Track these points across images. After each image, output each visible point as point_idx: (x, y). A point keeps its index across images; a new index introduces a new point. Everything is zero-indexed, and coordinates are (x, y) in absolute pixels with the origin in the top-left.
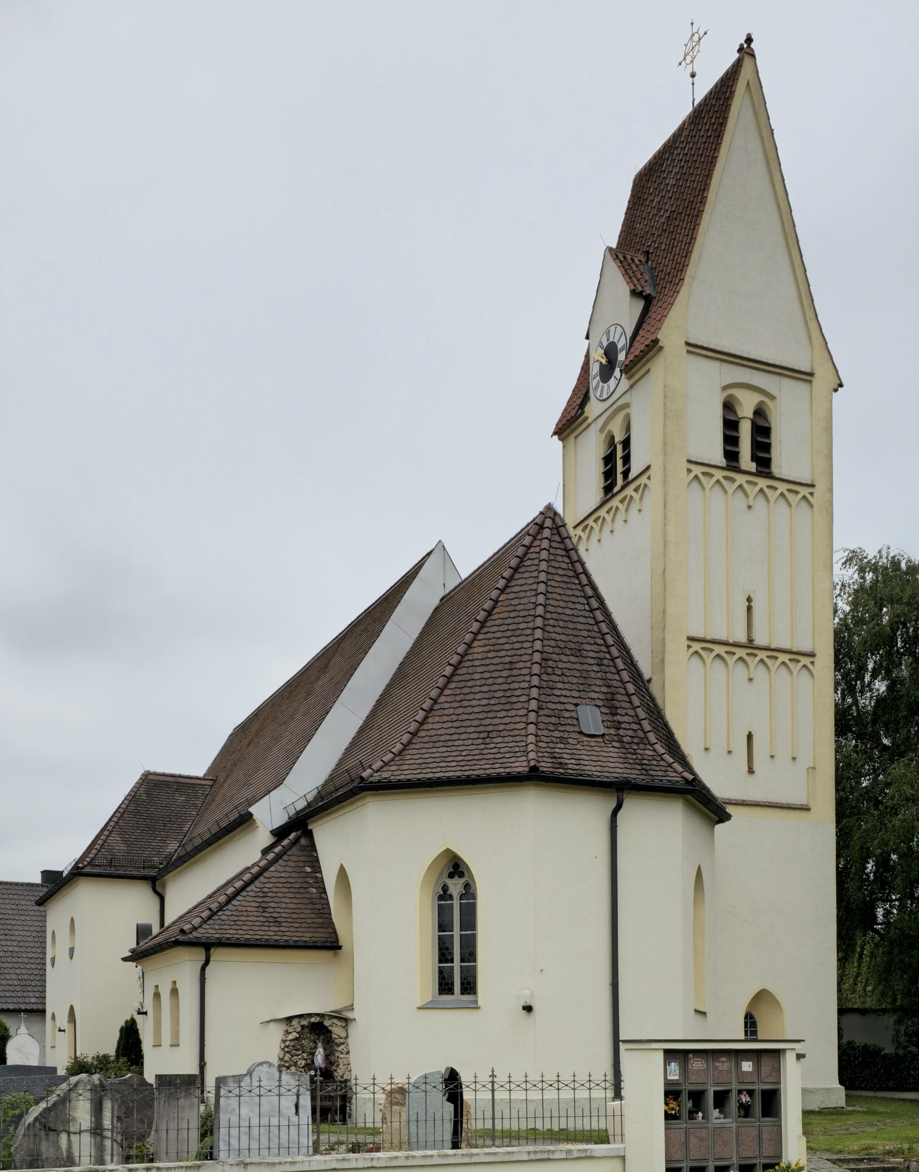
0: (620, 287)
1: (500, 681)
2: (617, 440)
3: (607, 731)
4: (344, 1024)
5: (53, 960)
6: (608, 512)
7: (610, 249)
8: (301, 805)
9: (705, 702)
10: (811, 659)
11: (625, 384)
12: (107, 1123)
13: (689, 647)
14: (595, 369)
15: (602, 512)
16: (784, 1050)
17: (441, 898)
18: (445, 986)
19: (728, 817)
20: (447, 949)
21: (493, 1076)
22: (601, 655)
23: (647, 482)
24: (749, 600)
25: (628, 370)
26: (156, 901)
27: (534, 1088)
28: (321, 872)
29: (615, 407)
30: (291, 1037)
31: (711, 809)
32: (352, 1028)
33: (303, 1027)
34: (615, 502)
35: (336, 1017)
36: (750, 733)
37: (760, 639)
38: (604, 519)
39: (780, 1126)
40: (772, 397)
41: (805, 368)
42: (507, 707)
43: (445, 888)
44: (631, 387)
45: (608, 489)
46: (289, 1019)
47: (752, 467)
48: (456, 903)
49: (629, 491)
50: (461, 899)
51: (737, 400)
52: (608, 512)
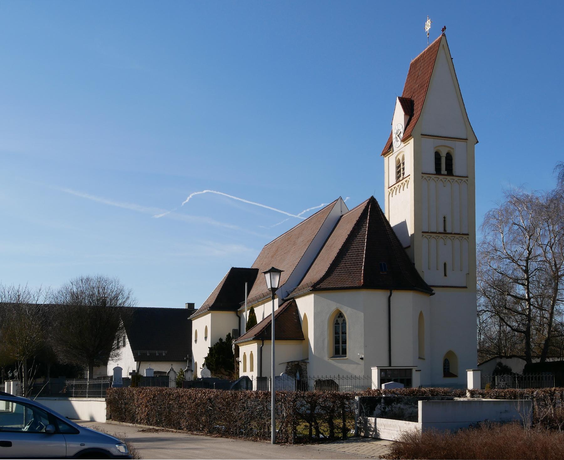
11: (403, 144)
17: (335, 324)
26: (238, 318)
32: (308, 365)
34: (400, 183)
40: (453, 149)
41: (464, 137)
43: (337, 321)
45: (398, 178)
46: (288, 363)
47: (446, 173)
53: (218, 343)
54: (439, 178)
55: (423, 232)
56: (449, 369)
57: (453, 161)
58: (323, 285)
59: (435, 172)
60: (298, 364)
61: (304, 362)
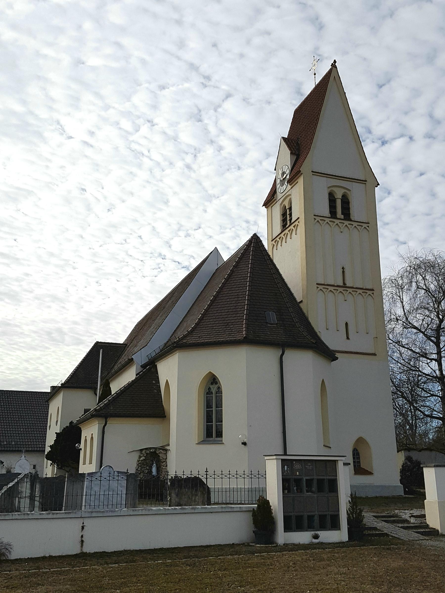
0: (287, 152)
1: (233, 302)
2: (287, 208)
3: (279, 322)
4: (165, 452)
5: (50, 426)
6: (284, 235)
7: (283, 138)
8: (153, 354)
9: (326, 309)
10: (372, 292)
11: (289, 187)
12: (37, 493)
13: (318, 287)
14: (278, 181)
15: (282, 235)
16: (338, 460)
17: (207, 394)
18: (209, 434)
19: (337, 358)
20: (210, 416)
21: (207, 471)
22: (277, 292)
23: (298, 224)
24: (343, 268)
25: (289, 182)
27: (226, 477)
28: (159, 383)
29: (286, 195)
30: (141, 459)
31: (330, 355)
33: (147, 454)
34: (286, 231)
35: (162, 449)
36: (347, 323)
37: (348, 285)
38: (283, 238)
39: (338, 496)
40: (349, 190)
42: (236, 313)
43: (209, 389)
44: (291, 188)
45: (284, 226)
46: (141, 450)
47: (342, 217)
48: (214, 396)
49: (292, 227)
50: (216, 394)
51: (334, 192)
52: (284, 235)
53: (67, 427)
54: (334, 222)
55: (317, 284)
56: (359, 462)
57: (350, 204)
58: (191, 340)
59: (330, 216)
60: (155, 452)
61: (163, 450)
